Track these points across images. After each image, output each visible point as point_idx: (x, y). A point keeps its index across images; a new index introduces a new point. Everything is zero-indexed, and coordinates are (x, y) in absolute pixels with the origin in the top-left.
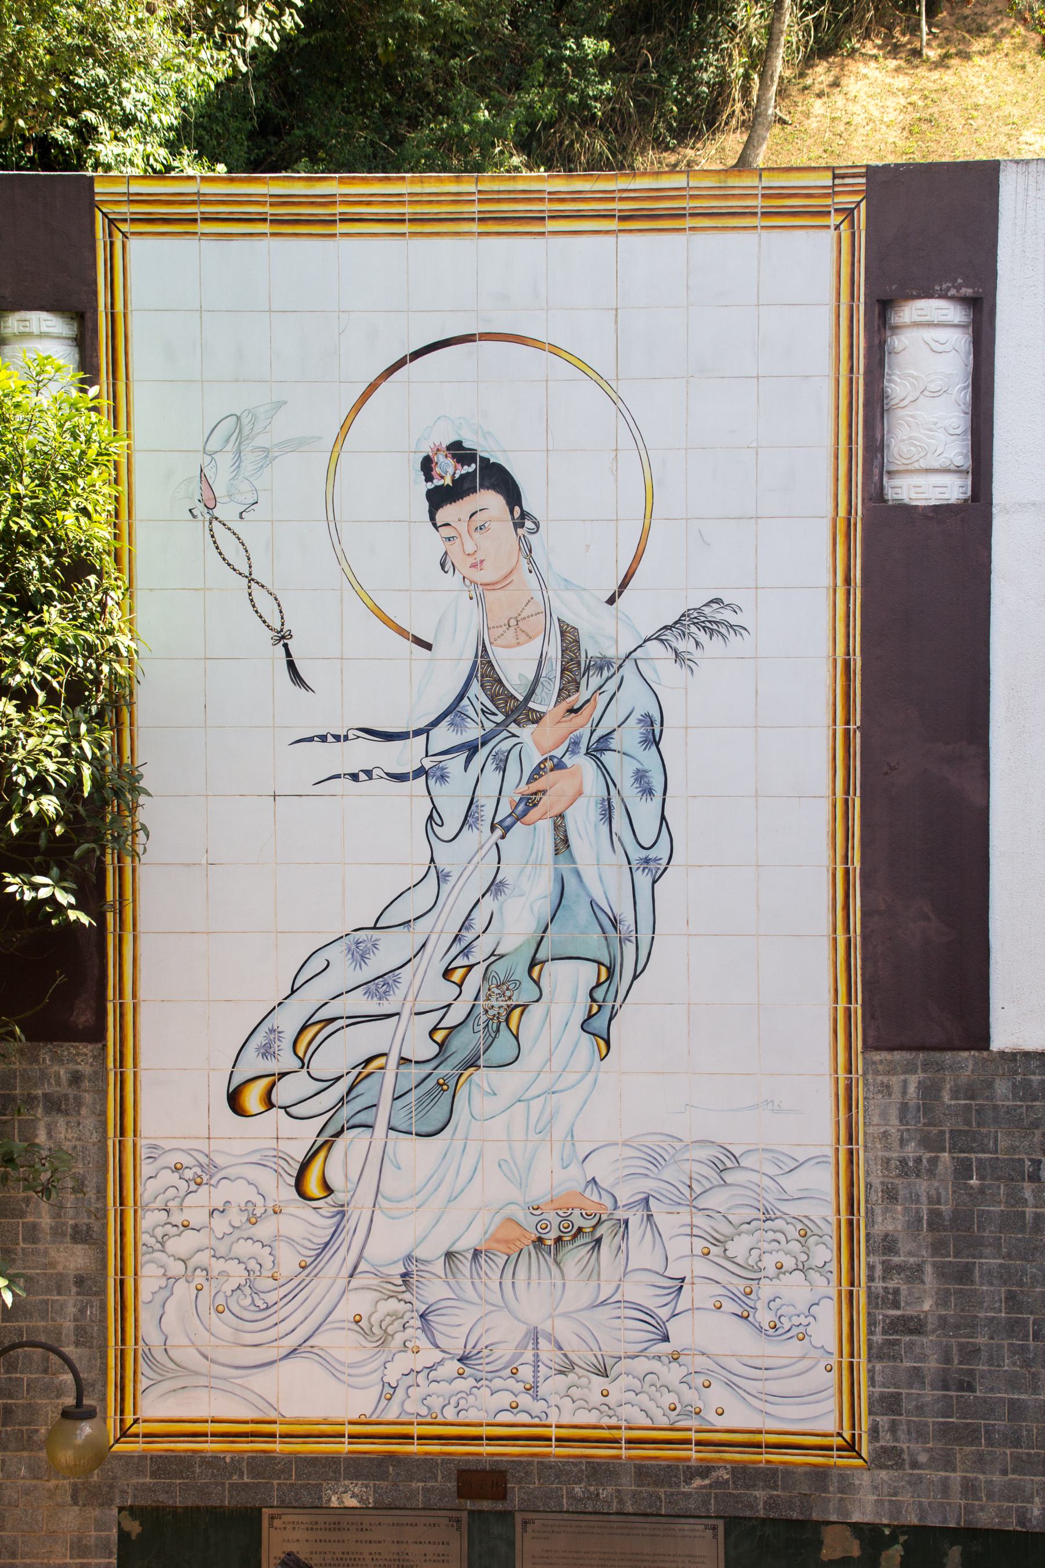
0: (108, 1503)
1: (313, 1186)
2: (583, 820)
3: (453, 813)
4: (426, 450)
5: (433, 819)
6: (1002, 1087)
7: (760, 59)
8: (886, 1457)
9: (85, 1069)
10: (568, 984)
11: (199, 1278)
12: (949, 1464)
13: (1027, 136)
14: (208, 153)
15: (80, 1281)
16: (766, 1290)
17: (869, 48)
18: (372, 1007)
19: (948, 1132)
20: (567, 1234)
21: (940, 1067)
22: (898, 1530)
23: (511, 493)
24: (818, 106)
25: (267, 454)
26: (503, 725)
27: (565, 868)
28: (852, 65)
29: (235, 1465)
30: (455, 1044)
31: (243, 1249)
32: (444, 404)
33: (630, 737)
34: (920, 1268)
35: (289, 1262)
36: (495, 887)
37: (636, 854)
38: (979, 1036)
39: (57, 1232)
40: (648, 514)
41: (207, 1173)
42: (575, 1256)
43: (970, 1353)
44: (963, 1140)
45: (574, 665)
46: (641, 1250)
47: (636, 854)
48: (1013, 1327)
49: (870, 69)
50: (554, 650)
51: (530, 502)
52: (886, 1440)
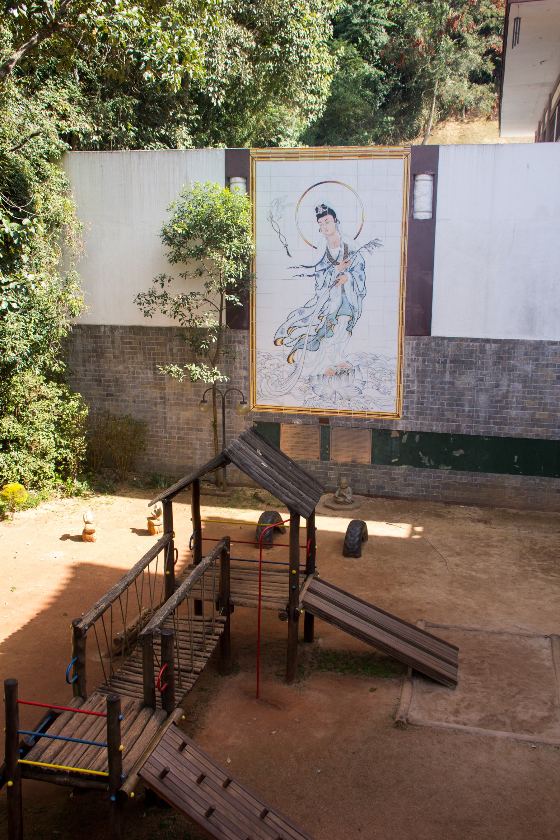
0: (251, 420)
1: (291, 361)
2: (348, 286)
3: (321, 284)
4: (317, 206)
5: (316, 285)
6: (433, 344)
7: (427, 122)
8: (405, 418)
9: (246, 335)
10: (344, 320)
11: (268, 378)
12: (417, 419)
13: (485, 139)
14: (304, 143)
15: (245, 377)
16: (382, 384)
17: (452, 119)
18: (303, 324)
19: (422, 353)
20: (343, 372)
21: (420, 339)
22: (406, 432)
23: (334, 215)
24: (440, 132)
25: (283, 207)
26: (331, 265)
27: (344, 296)
28: (447, 123)
29: (275, 415)
30: (320, 332)
31: (277, 373)
32: (320, 197)
33: (358, 268)
34: (414, 381)
35: (286, 376)
36: (329, 300)
37: (359, 293)
38: (429, 333)
39: (240, 368)
40: (363, 221)
41: (269, 357)
42: (344, 377)
43: (423, 398)
44: (424, 355)
45: (346, 253)
46: (357, 376)
47: (359, 293)
48: (432, 393)
49: (451, 124)
50: (342, 249)
51: (338, 217)
52: (405, 414)
